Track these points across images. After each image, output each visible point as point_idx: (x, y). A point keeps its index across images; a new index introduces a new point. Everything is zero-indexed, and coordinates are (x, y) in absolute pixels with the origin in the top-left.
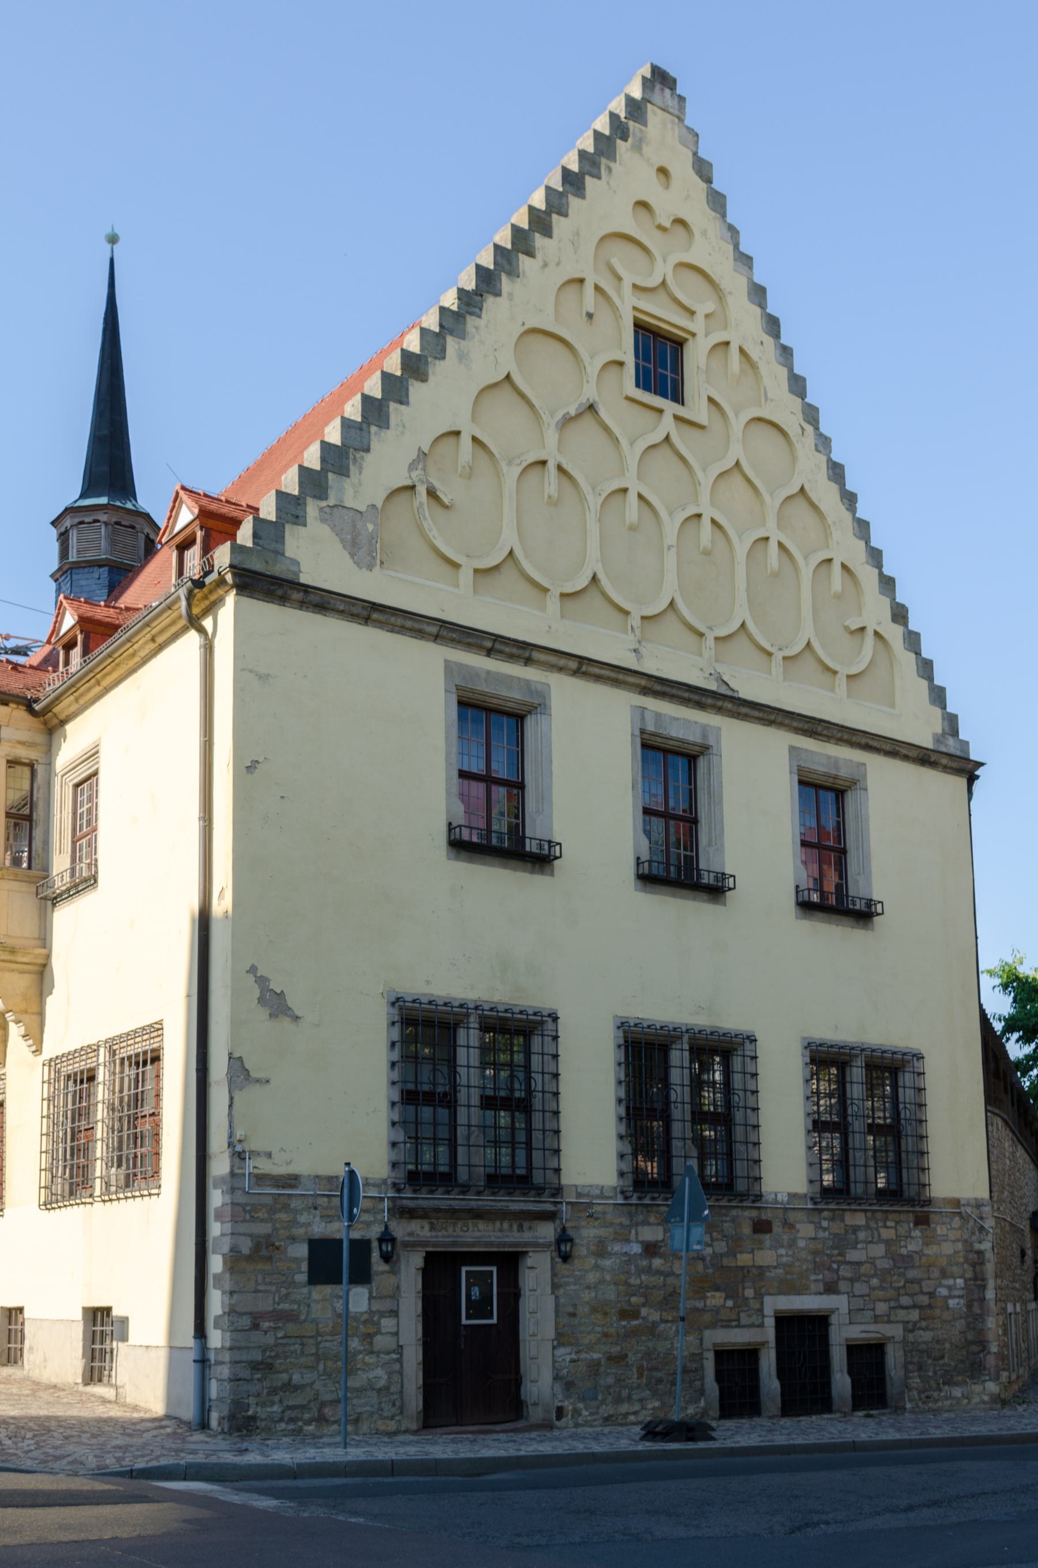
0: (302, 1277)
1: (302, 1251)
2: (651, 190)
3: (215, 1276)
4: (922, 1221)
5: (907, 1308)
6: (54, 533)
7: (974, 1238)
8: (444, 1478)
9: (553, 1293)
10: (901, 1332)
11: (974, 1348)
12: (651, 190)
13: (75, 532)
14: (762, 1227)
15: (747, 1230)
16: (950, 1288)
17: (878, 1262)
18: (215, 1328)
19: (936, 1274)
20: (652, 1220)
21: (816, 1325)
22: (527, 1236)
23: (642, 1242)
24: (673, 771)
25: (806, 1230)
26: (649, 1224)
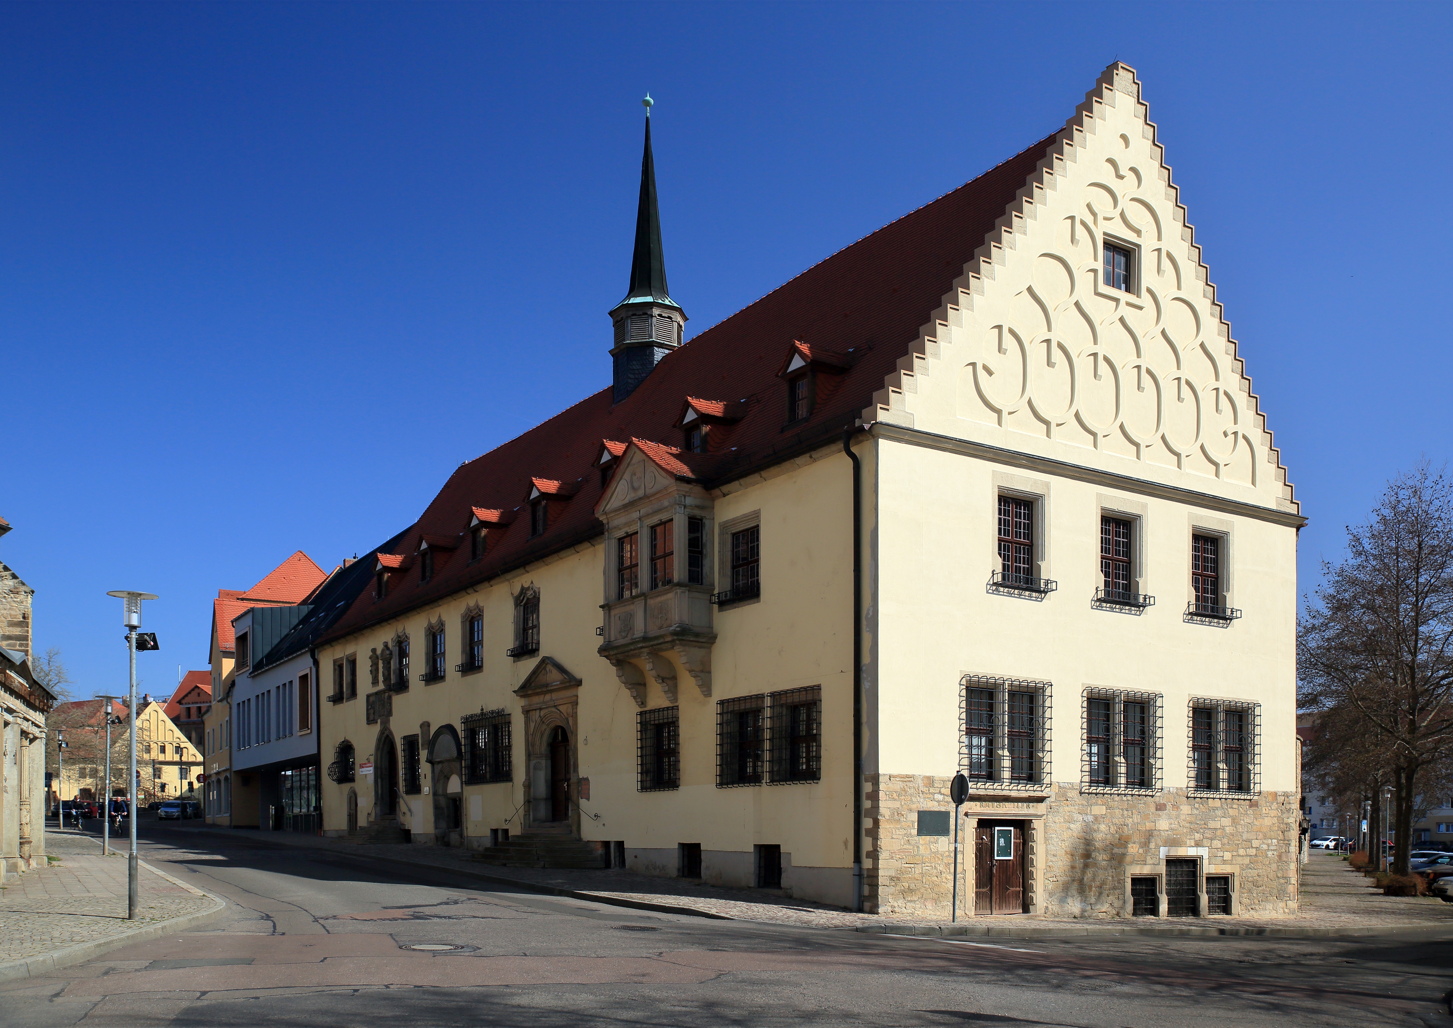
0: (915, 832)
1: (915, 817)
2: (1117, 150)
3: (866, 830)
4: (1253, 804)
5: (1242, 856)
6: (610, 321)
7: (1284, 815)
8: (212, 934)
9: (1045, 843)
10: (1238, 870)
11: (1282, 881)
12: (1117, 150)
13: (629, 321)
14: (1160, 807)
15: (1153, 809)
16: (1268, 845)
17: (1227, 829)
18: (867, 857)
19: (1261, 836)
20: (1100, 802)
21: (1192, 864)
22: (1031, 811)
23: (1094, 815)
24: (1119, 535)
25: (1185, 809)
26: (1097, 804)
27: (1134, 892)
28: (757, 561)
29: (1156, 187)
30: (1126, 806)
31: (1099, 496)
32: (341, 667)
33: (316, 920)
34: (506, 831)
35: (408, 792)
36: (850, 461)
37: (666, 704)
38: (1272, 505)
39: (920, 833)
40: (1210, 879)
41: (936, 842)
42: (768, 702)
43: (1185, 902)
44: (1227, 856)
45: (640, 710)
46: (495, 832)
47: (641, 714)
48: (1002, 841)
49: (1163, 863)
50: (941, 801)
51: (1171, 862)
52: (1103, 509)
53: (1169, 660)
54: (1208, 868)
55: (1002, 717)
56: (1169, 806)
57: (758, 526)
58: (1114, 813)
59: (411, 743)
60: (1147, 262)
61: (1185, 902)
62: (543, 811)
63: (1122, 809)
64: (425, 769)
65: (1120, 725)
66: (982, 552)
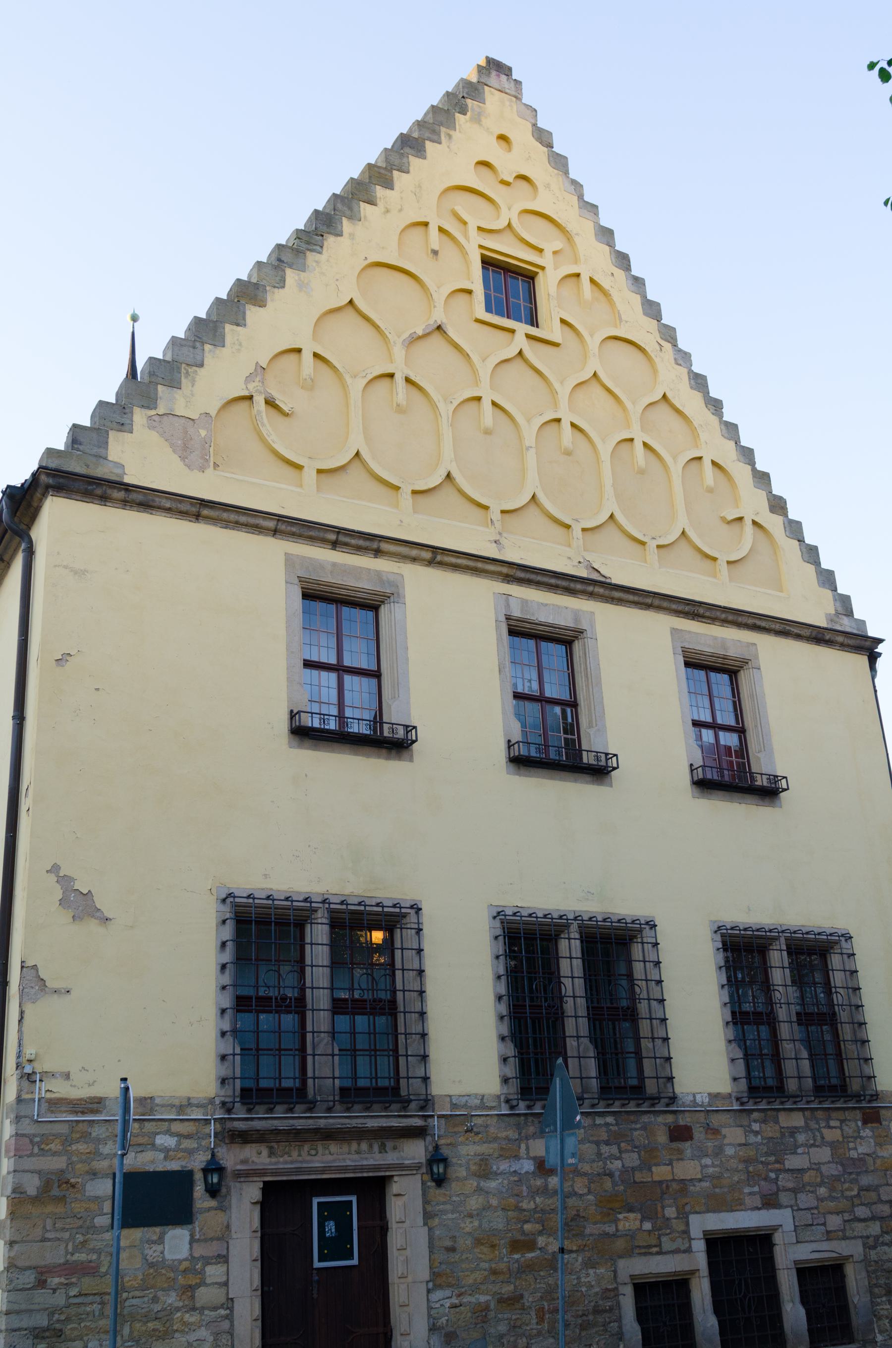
14: (680, 1134)
15: (662, 1138)
22: (391, 1158)
23: (534, 1159)
25: (733, 1135)
27: (641, 1316)
30: (605, 1136)
31: (290, 560)
40: (804, 1273)
41: (161, 1240)
44: (834, 1222)
48: (331, 1227)
54: (789, 1254)
56: (698, 1134)
60: (547, 287)
63: (598, 1143)
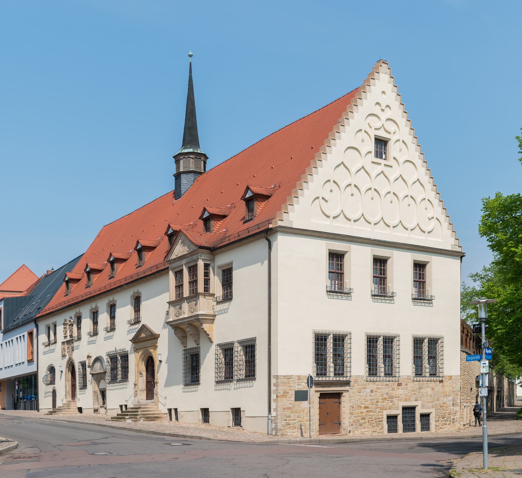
14: (399, 385)
28: (232, 283)
29: (397, 112)
32: (49, 328)
33: (55, 447)
34: (126, 406)
35: (395, 417)
36: (267, 242)
37: (195, 346)
38: (449, 248)
39: (295, 401)
42: (236, 345)
43: (409, 426)
45: (184, 348)
46: (121, 406)
47: (185, 350)
49: (401, 409)
50: (303, 386)
51: (404, 409)
52: (374, 255)
53: (403, 320)
55: (329, 348)
57: (232, 268)
58: (381, 386)
59: (83, 364)
61: (409, 426)
62: (144, 395)
64: (89, 377)
65: (380, 349)
66: (322, 277)
